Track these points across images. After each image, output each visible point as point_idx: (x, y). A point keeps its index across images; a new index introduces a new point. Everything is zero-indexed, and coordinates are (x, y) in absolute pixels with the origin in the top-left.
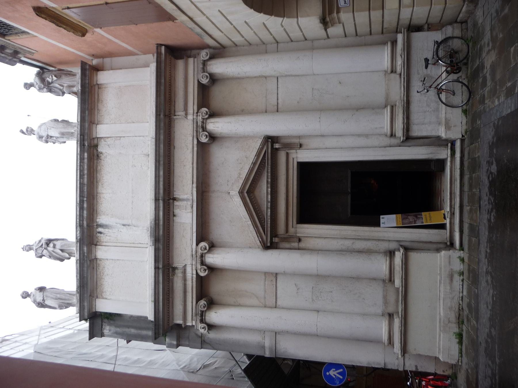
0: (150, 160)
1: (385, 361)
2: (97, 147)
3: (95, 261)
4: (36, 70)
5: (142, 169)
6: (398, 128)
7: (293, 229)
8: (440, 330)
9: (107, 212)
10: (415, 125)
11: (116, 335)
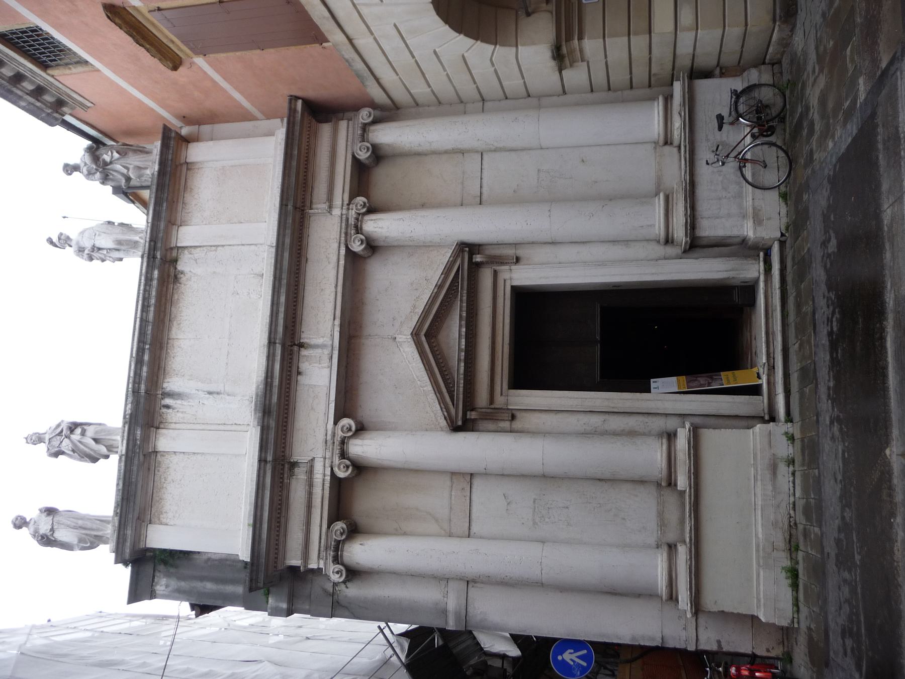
0: (263, 284)
1: (663, 634)
2: (176, 264)
3: (152, 457)
4: (87, 143)
5: (250, 298)
6: (677, 223)
7: (503, 397)
9: (183, 370)
10: (704, 219)
11: (177, 595)
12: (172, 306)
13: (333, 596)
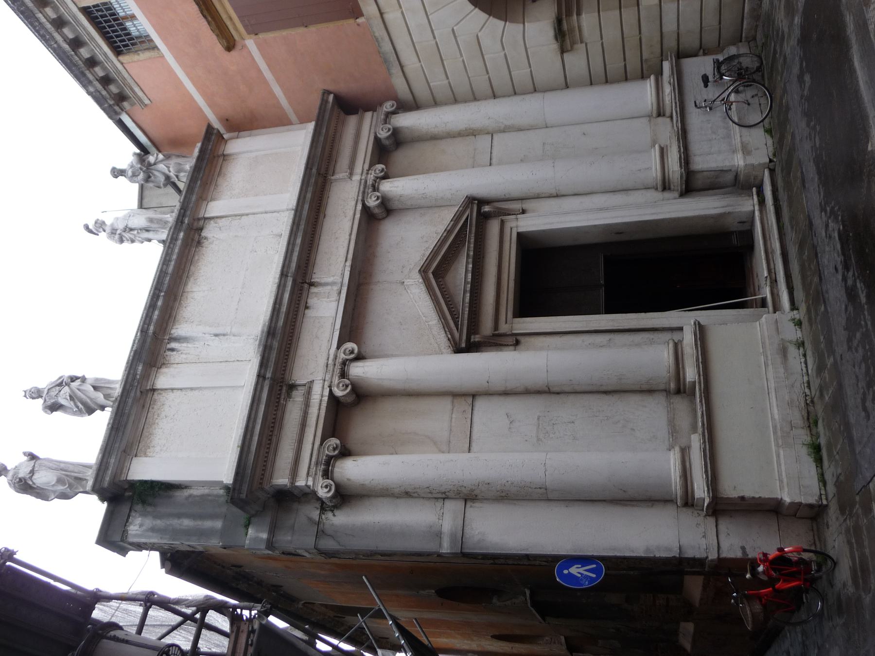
7: (507, 325)
8: (777, 445)
12: (192, 266)
13: (318, 525)
